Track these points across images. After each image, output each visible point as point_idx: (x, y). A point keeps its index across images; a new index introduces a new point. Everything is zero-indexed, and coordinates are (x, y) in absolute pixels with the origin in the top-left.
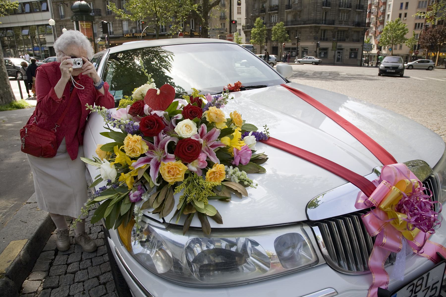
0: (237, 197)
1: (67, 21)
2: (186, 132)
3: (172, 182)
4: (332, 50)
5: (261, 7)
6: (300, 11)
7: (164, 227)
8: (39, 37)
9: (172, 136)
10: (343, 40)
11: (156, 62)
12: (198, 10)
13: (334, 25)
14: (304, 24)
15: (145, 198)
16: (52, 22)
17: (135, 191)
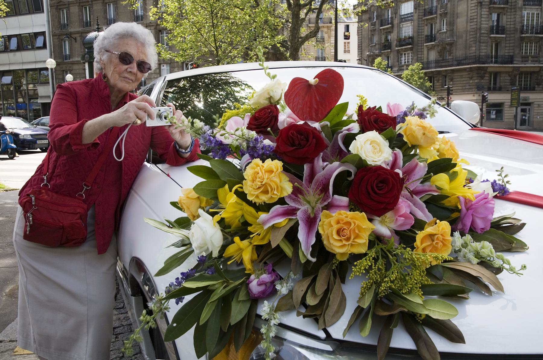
0: (479, 292)
1: (73, 63)
2: (372, 155)
3: (343, 254)
4: (511, 106)
5: (383, 41)
6: (451, 44)
7: (328, 348)
8: (27, 87)
9: (343, 163)
10: (532, 89)
11: (228, 105)
12: (283, 46)
13: (512, 63)
14: (458, 65)
15: (283, 289)
16: (51, 63)
17: (262, 274)
